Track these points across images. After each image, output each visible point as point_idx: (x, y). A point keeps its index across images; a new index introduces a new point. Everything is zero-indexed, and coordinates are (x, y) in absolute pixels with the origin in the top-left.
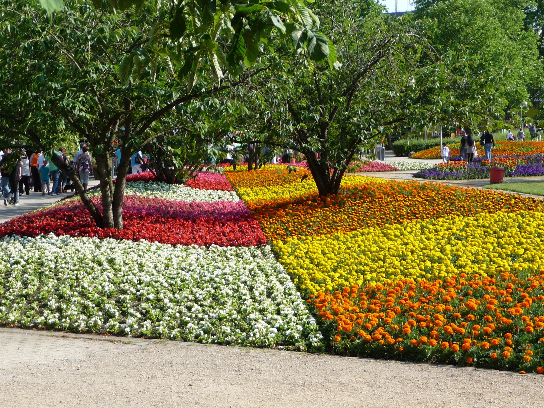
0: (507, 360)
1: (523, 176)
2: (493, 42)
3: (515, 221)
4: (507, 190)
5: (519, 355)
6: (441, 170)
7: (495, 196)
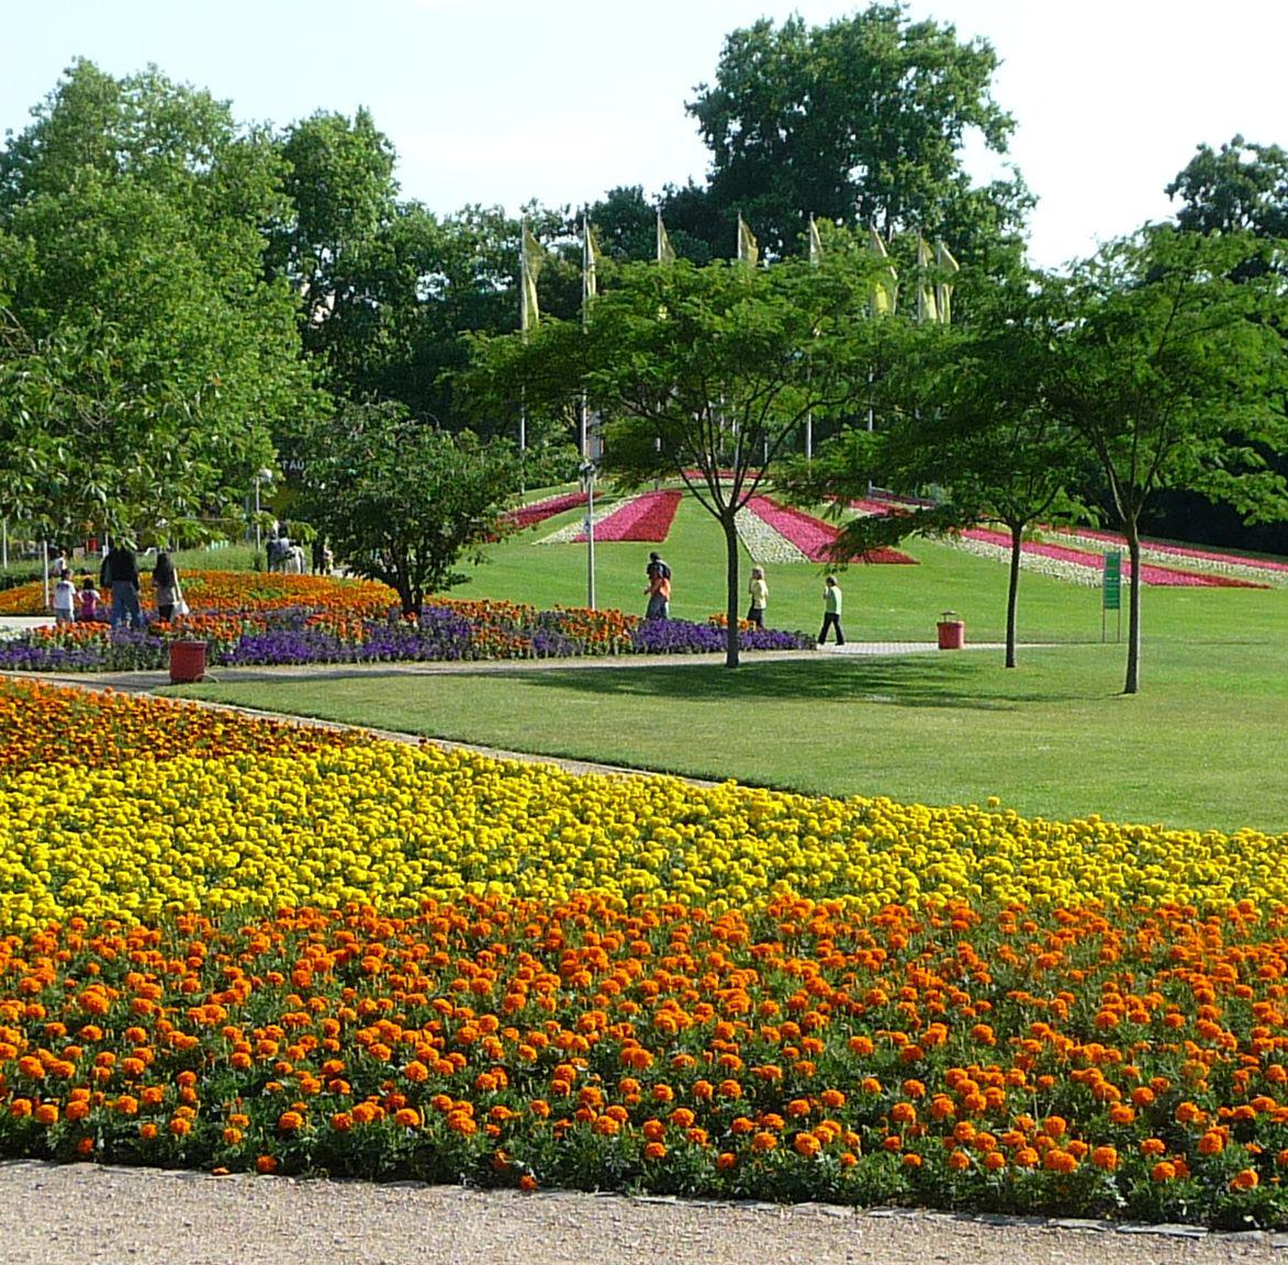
0: (183, 1141)
1: (257, 663)
2: (183, 309)
3: (220, 782)
4: (213, 701)
5: (214, 1128)
6: (42, 644)
7: (176, 715)
